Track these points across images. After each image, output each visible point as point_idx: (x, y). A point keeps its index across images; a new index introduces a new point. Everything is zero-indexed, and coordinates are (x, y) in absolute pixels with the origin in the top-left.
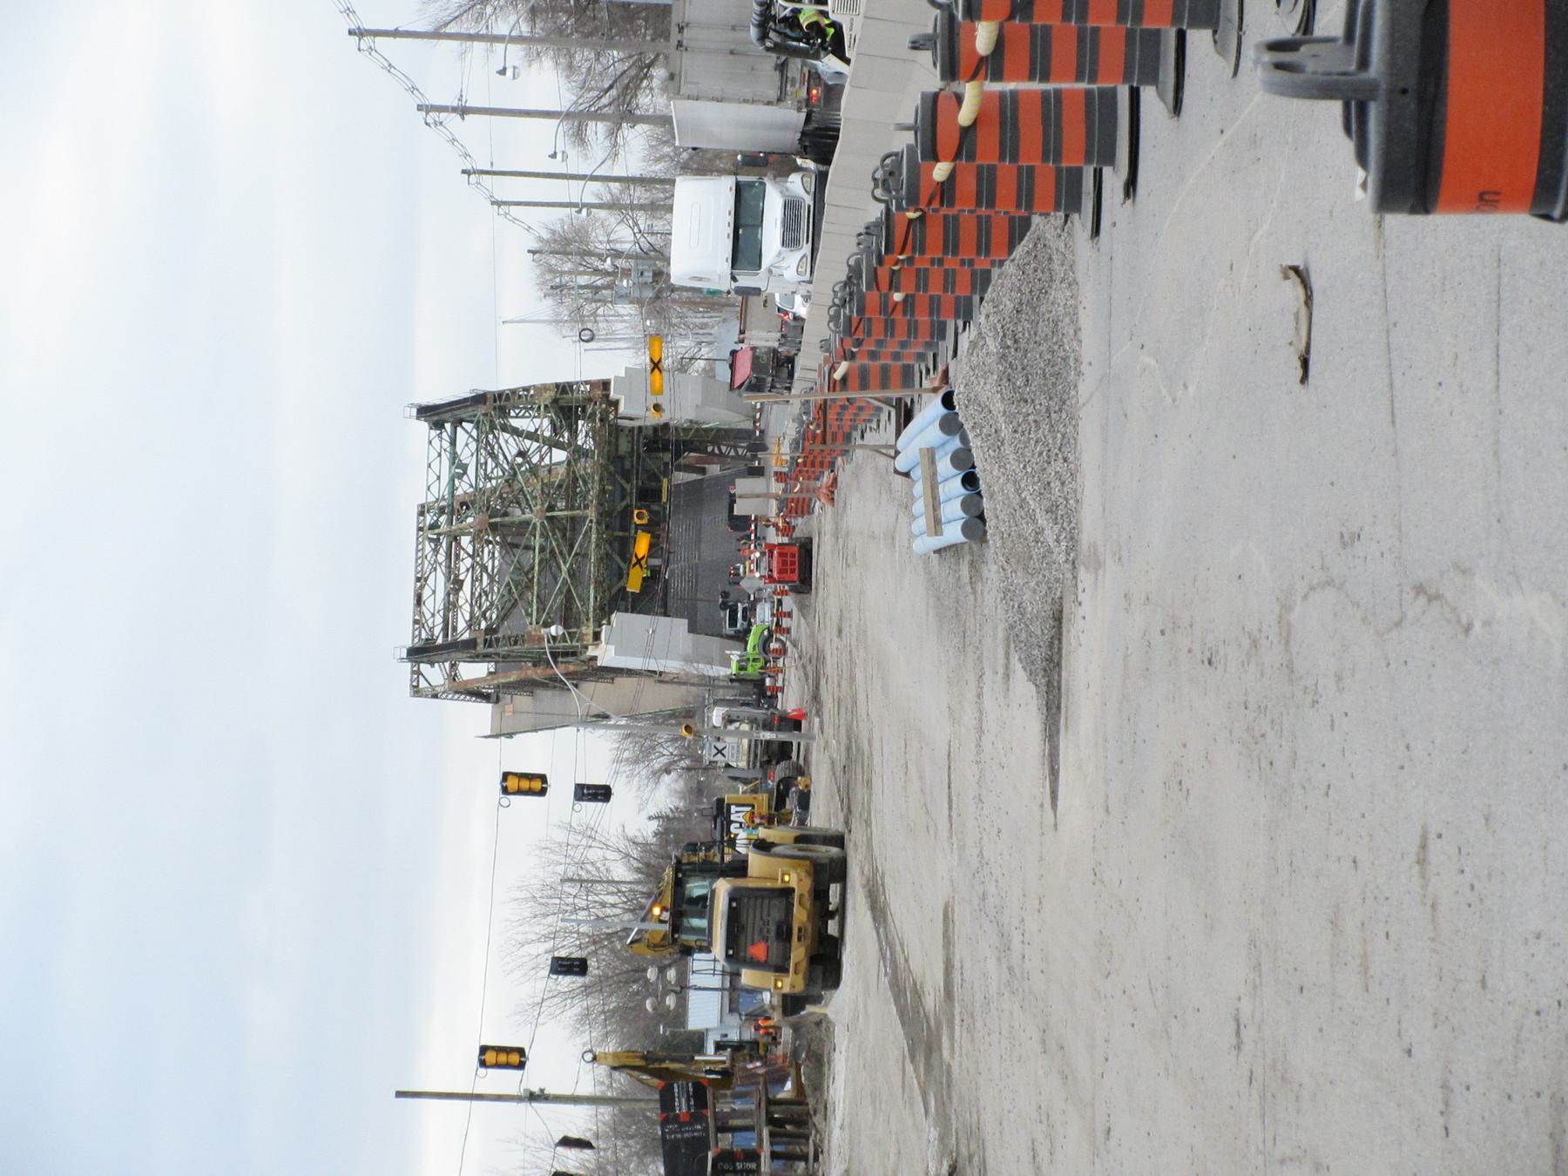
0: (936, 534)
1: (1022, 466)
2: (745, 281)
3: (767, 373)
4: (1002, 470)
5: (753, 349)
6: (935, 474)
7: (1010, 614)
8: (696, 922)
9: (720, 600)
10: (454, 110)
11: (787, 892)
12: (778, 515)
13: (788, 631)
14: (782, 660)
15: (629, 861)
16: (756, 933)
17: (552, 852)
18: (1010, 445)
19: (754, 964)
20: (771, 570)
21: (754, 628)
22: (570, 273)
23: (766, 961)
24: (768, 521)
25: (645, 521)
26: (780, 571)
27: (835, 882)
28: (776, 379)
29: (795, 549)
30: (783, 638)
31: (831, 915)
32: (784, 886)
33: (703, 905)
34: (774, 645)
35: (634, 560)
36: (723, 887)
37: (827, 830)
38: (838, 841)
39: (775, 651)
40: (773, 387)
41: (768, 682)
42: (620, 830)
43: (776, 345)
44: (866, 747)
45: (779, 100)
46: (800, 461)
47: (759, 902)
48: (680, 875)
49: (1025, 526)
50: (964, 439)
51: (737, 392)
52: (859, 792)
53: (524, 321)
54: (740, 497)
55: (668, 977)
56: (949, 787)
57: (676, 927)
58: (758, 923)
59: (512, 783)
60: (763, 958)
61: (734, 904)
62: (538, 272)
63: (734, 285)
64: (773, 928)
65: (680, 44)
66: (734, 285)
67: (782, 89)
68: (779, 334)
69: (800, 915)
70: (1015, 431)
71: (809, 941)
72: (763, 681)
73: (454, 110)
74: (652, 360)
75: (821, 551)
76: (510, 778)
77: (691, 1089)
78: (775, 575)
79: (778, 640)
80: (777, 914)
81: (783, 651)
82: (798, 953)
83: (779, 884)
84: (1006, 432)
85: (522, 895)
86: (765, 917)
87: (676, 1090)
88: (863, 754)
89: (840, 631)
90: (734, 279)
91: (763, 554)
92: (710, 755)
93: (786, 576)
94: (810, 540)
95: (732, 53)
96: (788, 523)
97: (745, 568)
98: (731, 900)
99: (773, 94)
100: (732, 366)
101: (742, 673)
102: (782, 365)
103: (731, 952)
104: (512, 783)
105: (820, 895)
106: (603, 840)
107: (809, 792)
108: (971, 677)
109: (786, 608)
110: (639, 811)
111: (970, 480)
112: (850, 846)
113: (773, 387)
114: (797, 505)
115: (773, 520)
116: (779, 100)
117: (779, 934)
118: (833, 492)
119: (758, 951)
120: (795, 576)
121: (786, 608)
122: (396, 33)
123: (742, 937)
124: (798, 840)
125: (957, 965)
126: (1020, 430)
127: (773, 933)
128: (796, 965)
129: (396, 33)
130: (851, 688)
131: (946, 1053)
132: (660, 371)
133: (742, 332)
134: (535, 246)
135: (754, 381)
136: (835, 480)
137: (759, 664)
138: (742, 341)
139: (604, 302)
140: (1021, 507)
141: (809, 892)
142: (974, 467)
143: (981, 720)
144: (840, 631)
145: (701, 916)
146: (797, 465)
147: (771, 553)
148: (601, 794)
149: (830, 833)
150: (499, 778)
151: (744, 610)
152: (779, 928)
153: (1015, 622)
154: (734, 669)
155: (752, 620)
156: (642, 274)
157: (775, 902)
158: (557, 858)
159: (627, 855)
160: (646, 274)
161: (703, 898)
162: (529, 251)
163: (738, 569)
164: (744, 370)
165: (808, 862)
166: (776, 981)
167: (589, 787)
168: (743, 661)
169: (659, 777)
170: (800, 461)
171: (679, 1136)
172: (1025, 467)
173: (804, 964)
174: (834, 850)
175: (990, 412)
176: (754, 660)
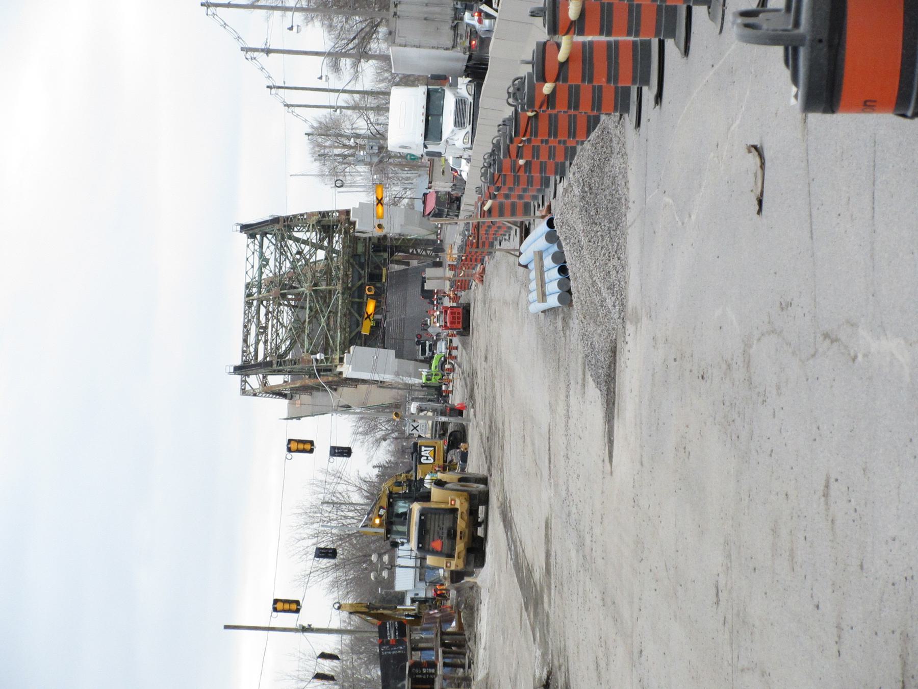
0: (543, 302)
1: (593, 262)
2: (432, 148)
3: (444, 206)
4: (582, 264)
5: (437, 192)
6: (542, 266)
7: (586, 349)
8: (400, 528)
9: (416, 340)
10: (262, 50)
11: (454, 511)
12: (450, 290)
13: (456, 357)
14: (452, 374)
15: (361, 492)
16: (436, 534)
17: (317, 486)
18: (587, 250)
19: (434, 553)
20: (446, 322)
21: (435, 356)
22: (330, 147)
23: (441, 551)
24: (445, 293)
25: (372, 293)
26: (452, 323)
27: (482, 505)
28: (450, 210)
29: (460, 310)
30: (453, 362)
31: (480, 524)
32: (452, 507)
33: (405, 517)
34: (447, 366)
35: (366, 316)
36: (416, 507)
37: (477, 474)
38: (484, 481)
39: (448, 369)
40: (448, 215)
41: (444, 387)
42: (356, 473)
43: (450, 190)
44: (500, 426)
45: (453, 47)
46: (463, 258)
47: (437, 517)
48: (391, 500)
49: (595, 297)
50: (560, 246)
51: (427, 218)
52: (497, 452)
53: (303, 175)
54: (428, 279)
55: (384, 560)
56: (549, 450)
57: (389, 531)
58: (437, 529)
59: (294, 446)
60: (439, 549)
61: (423, 518)
62: (311, 146)
63: (426, 150)
64: (445, 532)
65: (395, 14)
66: (426, 150)
67: (455, 40)
68: (452, 184)
69: (461, 524)
70: (590, 241)
71: (466, 540)
72: (441, 387)
73: (262, 50)
74: (377, 198)
75: (476, 312)
76: (292, 442)
77: (397, 625)
78: (448, 325)
79: (450, 363)
80: (447, 524)
81: (453, 370)
82: (460, 546)
83: (449, 506)
84: (584, 241)
85: (300, 511)
86: (441, 526)
87: (388, 626)
88: (499, 430)
89: (486, 358)
90: (425, 147)
91: (441, 312)
92: (409, 430)
93: (455, 326)
94: (469, 305)
95: (426, 19)
96: (456, 295)
97: (431, 320)
98: (421, 515)
99: (450, 44)
100: (424, 203)
101: (428, 382)
102: (454, 202)
103: (421, 545)
104: (294, 446)
105: (473, 512)
106: (347, 479)
107: (467, 452)
108: (562, 385)
109: (454, 345)
110: (368, 462)
111: (563, 270)
112: (491, 484)
113: (448, 215)
114: (461, 284)
115: (447, 293)
116: (453, 47)
117: (449, 535)
118: (482, 277)
119: (437, 545)
120: (460, 326)
121: (454, 345)
122: (229, 5)
123: (428, 536)
124: (460, 480)
125: (553, 554)
126: (592, 240)
127: (445, 535)
128: (459, 554)
129: (229, 5)
130: (492, 391)
131: (546, 606)
132: (382, 204)
133: (430, 182)
134: (309, 131)
135: (437, 211)
136: (484, 269)
137: (438, 378)
138: (430, 188)
139: (350, 164)
140: (593, 286)
141: (467, 511)
142: (565, 262)
143: (568, 411)
144: (486, 358)
145: (403, 524)
146: (462, 260)
147: (446, 311)
148: (346, 453)
149: (479, 476)
150: (286, 443)
151: (430, 345)
152: (449, 531)
153: (589, 353)
154: (424, 380)
155: (435, 351)
156: (372, 148)
157: (447, 516)
158: (319, 490)
159: (360, 489)
160: (374, 148)
161: (405, 514)
162: (306, 134)
163: (427, 320)
164: (431, 204)
165: (466, 494)
166: (447, 563)
167: (339, 448)
168: (429, 375)
169: (380, 443)
170: (463, 258)
171: (389, 653)
172: (595, 262)
173: (463, 554)
174: (482, 486)
175: (575, 230)
176: (436, 375)
